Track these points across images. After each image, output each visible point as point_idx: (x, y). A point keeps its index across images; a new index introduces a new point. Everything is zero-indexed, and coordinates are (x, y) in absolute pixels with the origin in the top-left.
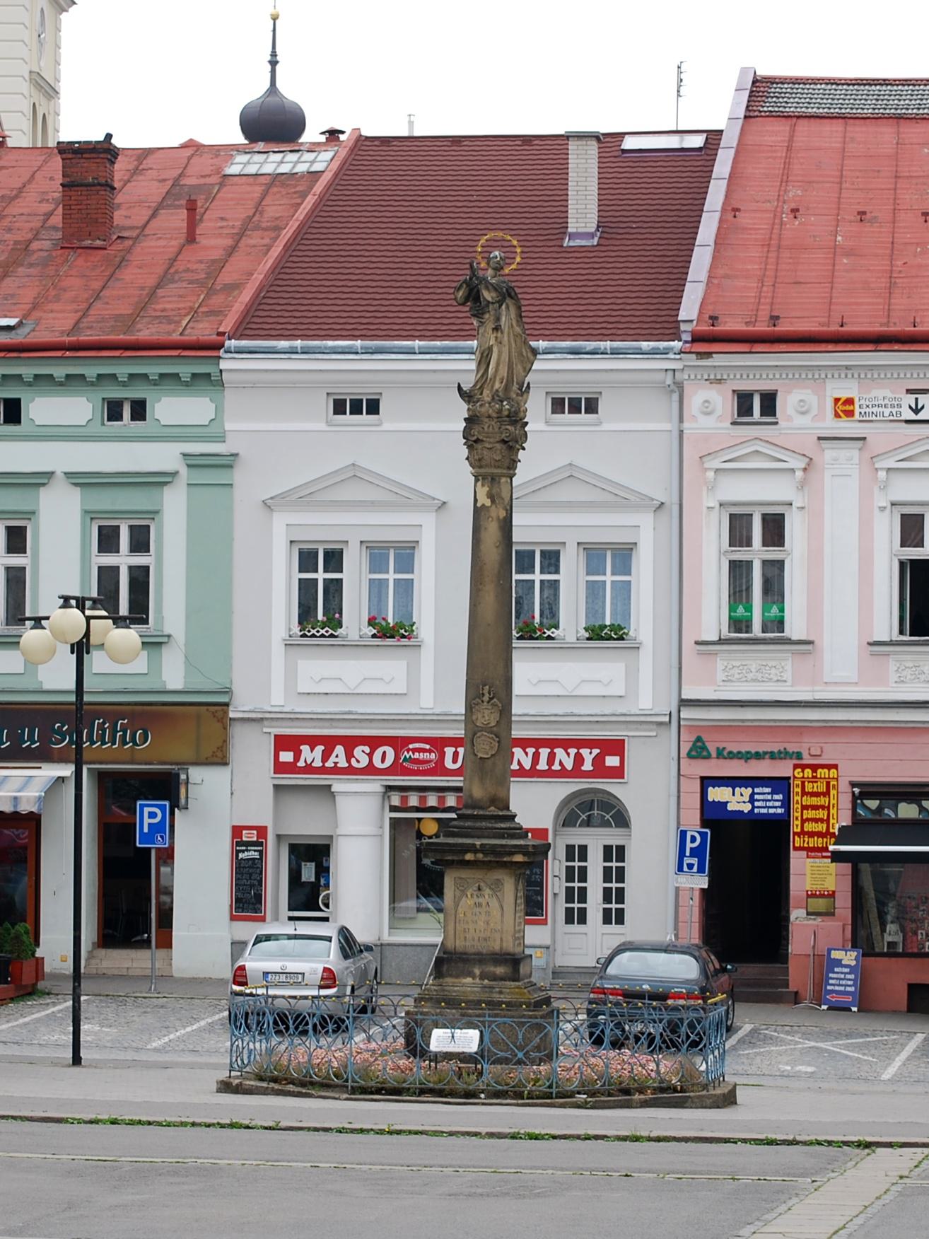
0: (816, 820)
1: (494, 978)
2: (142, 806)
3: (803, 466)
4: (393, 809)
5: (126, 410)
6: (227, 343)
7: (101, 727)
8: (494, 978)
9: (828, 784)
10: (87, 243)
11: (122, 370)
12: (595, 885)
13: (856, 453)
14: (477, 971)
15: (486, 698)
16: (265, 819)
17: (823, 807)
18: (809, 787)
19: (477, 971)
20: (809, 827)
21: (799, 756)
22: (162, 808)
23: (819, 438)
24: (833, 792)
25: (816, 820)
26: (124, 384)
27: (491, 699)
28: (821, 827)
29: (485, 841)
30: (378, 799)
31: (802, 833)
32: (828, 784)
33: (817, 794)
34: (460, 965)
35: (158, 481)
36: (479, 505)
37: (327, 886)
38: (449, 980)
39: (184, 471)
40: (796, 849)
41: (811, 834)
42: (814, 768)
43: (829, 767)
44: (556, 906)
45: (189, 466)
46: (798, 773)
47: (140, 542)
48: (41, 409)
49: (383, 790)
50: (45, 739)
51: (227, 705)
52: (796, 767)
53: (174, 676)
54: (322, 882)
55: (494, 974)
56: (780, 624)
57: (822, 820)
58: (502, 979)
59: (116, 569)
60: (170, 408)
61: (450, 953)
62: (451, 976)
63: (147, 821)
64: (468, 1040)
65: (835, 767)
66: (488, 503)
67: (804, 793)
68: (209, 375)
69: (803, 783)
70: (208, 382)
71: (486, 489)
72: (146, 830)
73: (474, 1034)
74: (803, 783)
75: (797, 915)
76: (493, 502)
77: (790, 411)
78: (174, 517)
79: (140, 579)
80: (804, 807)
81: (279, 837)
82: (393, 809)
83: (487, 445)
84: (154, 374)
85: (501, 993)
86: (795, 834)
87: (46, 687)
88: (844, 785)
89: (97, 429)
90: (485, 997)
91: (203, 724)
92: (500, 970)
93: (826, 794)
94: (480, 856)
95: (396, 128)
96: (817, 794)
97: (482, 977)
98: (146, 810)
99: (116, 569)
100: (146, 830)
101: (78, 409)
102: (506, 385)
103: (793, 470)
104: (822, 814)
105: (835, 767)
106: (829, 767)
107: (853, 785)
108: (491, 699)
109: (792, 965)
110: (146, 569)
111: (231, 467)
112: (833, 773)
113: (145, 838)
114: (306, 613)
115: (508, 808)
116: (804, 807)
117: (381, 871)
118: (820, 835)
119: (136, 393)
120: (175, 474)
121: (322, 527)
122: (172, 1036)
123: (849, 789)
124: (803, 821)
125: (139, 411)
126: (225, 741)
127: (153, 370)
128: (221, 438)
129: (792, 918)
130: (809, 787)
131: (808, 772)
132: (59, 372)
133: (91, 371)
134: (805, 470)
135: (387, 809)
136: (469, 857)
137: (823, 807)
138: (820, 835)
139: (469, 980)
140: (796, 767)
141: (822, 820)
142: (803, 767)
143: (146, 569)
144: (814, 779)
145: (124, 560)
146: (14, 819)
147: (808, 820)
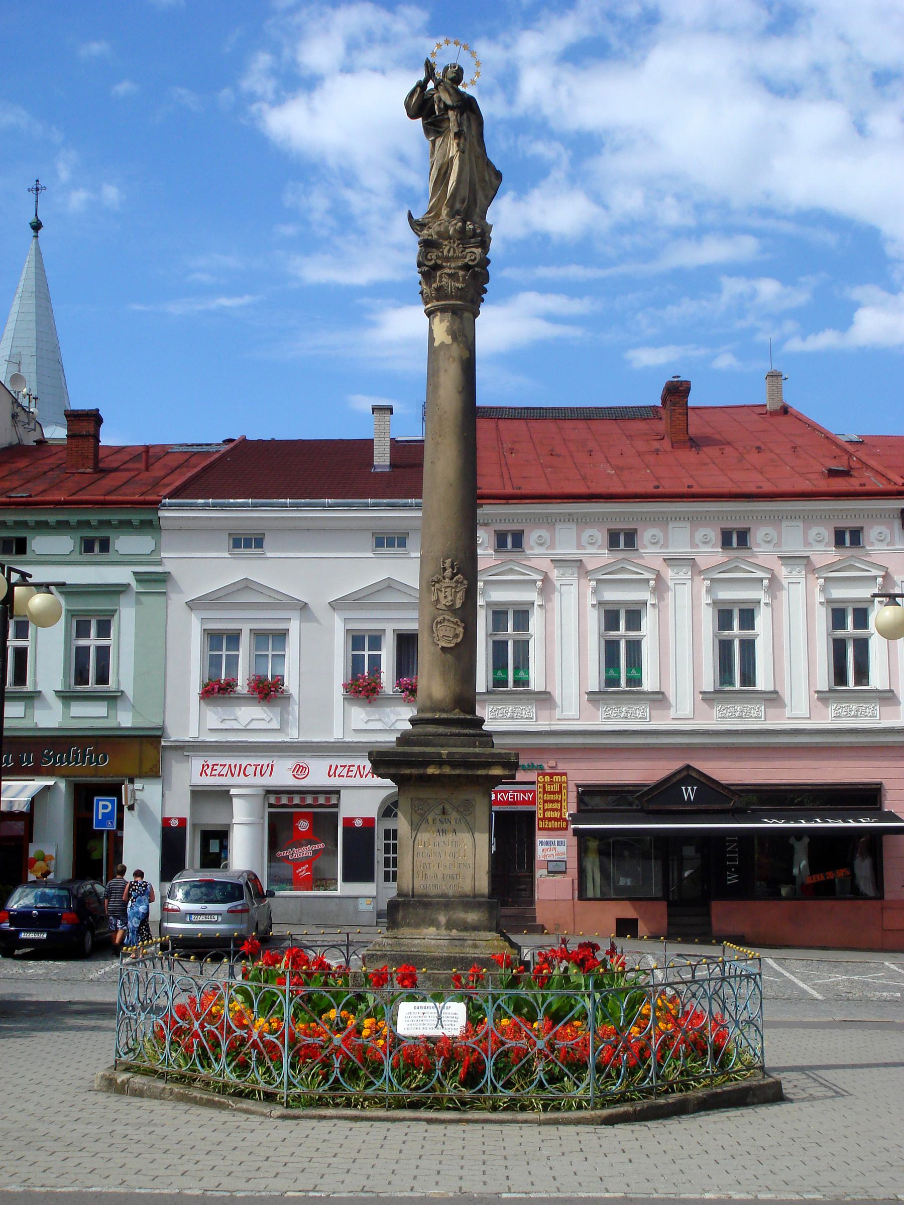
0: (553, 810)
1: (466, 927)
2: (98, 801)
3: (542, 578)
4: (271, 806)
5: (95, 546)
6: (164, 501)
7: (75, 752)
8: (466, 927)
9: (561, 786)
10: (82, 470)
11: (93, 518)
12: (379, 856)
13: (576, 570)
14: (442, 919)
15: (448, 573)
16: (186, 814)
17: (557, 801)
18: (548, 788)
19: (442, 919)
20: (548, 814)
21: (540, 768)
22: (112, 802)
23: (552, 561)
24: (564, 791)
25: (553, 810)
26: (96, 528)
27: (454, 575)
28: (556, 815)
29: (454, 750)
30: (259, 801)
31: (544, 819)
32: (561, 786)
33: (553, 793)
34: (421, 911)
35: (116, 591)
36: (436, 344)
37: (226, 858)
38: (406, 931)
39: (134, 584)
40: (540, 829)
41: (550, 819)
42: (551, 775)
43: (561, 774)
44: (379, 870)
45: (137, 581)
46: (541, 779)
47: (104, 630)
48: (39, 544)
49: (264, 793)
50: (37, 760)
51: (160, 737)
52: (539, 775)
53: (125, 719)
54: (223, 856)
55: (465, 922)
56: (526, 683)
57: (557, 810)
58: (475, 928)
59: (87, 648)
60: (124, 544)
61: (406, 896)
62: (409, 925)
63: (101, 811)
64: (452, 1019)
65: (565, 774)
66: (448, 340)
67: (545, 792)
68: (151, 521)
69: (544, 785)
70: (150, 526)
71: (446, 324)
72: (100, 817)
73: (503, 1023)
74: (544, 785)
75: (540, 873)
76: (454, 338)
77: (532, 543)
78: (127, 618)
79: (103, 653)
80: (545, 802)
81: (194, 826)
82: (271, 806)
83: (448, 271)
84: (114, 520)
85: (475, 946)
86: (539, 819)
87: (41, 726)
88: (572, 788)
89: (76, 557)
90: (456, 952)
91: (145, 751)
92: (472, 917)
93: (560, 792)
94: (447, 770)
95: (267, 437)
96: (553, 793)
97: (450, 926)
98: (101, 803)
99: (87, 648)
100: (100, 817)
101: (64, 544)
102: (468, 206)
103: (535, 582)
104: (556, 806)
105: (565, 774)
106: (561, 774)
107: (578, 786)
108: (454, 575)
109: (538, 907)
110: (107, 648)
111: (165, 581)
112: (564, 778)
113: (99, 822)
114: (81, 677)
115: (473, 712)
116: (545, 802)
117: (263, 847)
118: (556, 819)
119: (103, 534)
120: (128, 585)
121: (223, 621)
122: (107, 969)
123: (575, 789)
124: (544, 811)
125: (105, 546)
126: (158, 761)
127: (115, 517)
128: (159, 563)
129: (537, 875)
130: (548, 788)
131: (547, 778)
132: (52, 519)
133: (73, 518)
134: (542, 581)
135: (267, 806)
136: (430, 771)
137: (557, 801)
138: (556, 819)
139: (432, 930)
140: (539, 775)
141: (557, 810)
142: (544, 775)
143: (107, 648)
144: (551, 783)
145: (92, 642)
146: (11, 816)
147: (548, 810)
